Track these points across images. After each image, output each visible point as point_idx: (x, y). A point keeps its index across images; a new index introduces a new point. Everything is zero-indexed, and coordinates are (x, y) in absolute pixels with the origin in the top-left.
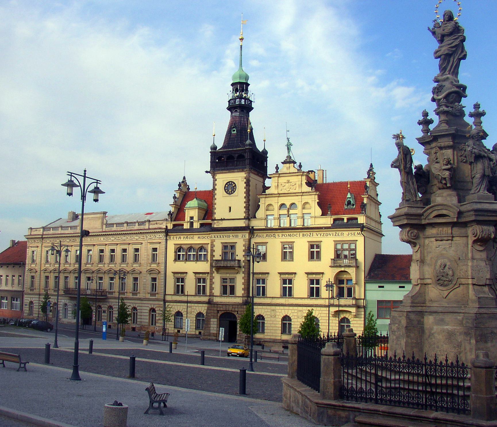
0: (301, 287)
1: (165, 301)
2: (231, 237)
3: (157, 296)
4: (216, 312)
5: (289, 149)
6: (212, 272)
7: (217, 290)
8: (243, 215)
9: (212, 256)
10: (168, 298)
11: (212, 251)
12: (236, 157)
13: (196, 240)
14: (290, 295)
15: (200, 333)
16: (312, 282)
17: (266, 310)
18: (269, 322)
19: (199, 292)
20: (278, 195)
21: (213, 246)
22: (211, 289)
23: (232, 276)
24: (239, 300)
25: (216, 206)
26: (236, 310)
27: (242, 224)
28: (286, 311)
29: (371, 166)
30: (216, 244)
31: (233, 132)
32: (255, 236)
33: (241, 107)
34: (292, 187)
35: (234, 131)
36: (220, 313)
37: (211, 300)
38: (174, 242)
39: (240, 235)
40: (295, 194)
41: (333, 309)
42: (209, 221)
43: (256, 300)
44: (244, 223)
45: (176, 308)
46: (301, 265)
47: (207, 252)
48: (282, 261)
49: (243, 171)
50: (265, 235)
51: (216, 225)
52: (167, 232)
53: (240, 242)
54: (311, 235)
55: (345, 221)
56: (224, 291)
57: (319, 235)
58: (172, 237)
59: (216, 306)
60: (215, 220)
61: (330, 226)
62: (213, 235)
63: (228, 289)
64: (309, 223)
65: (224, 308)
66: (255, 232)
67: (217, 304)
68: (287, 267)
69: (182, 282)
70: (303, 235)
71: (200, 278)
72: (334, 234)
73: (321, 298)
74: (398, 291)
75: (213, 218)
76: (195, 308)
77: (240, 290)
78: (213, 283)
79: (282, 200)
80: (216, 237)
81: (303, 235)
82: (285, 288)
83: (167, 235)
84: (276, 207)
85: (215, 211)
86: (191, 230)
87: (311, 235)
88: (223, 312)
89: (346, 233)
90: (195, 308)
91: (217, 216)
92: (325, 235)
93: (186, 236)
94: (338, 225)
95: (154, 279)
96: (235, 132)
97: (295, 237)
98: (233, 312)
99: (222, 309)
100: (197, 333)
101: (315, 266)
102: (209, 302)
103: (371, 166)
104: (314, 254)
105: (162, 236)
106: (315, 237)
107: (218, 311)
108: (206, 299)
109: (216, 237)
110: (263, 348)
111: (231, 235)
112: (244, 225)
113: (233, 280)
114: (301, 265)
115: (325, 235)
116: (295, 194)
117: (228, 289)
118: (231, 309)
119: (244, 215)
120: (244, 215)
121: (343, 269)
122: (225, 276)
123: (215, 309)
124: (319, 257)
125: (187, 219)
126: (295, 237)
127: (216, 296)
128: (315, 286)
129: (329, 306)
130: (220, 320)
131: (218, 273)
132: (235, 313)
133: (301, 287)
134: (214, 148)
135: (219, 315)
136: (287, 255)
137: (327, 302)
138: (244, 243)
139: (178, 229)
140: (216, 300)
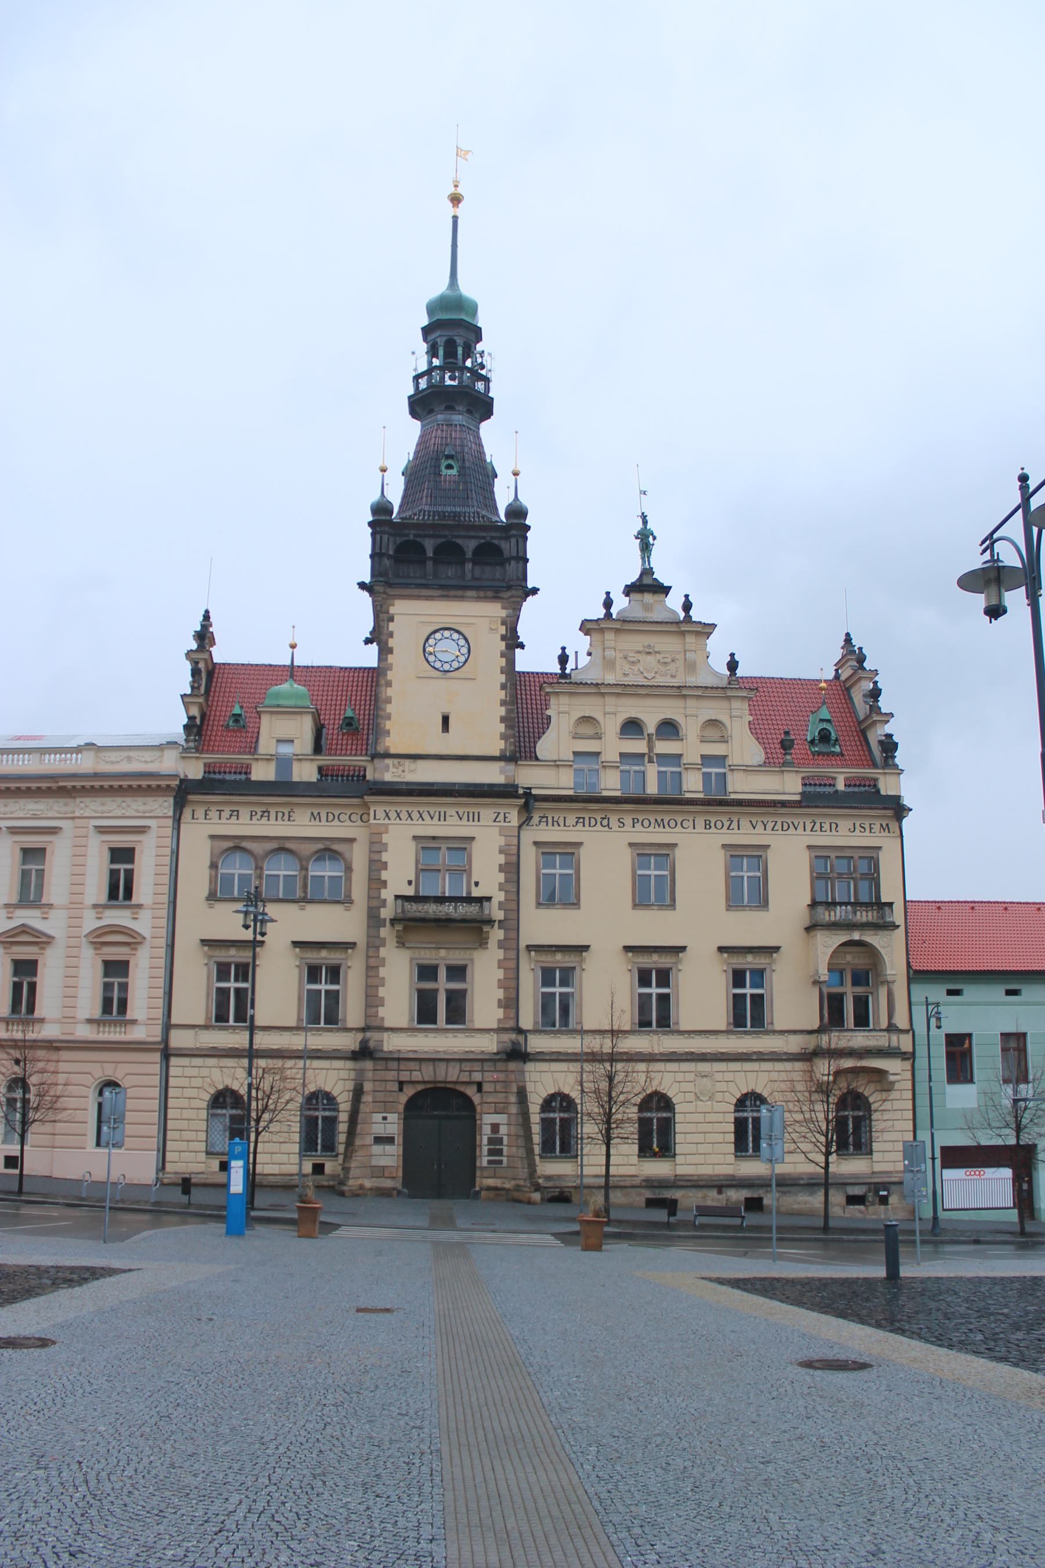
0: (702, 997)
1: (167, 1053)
2: (453, 820)
3: (138, 1034)
4: (395, 1087)
5: (646, 548)
6: (374, 944)
7: (398, 1003)
8: (496, 746)
9: (376, 883)
10: (179, 1039)
11: (376, 866)
12: (469, 554)
13: (303, 824)
14: (758, 1020)
15: (318, 1169)
16: (738, 978)
17: (680, 1077)
18: (690, 1117)
19: (221, 1017)
20: (684, 692)
21: (376, 847)
22: (372, 1000)
23: (456, 957)
24: (489, 1044)
25: (389, 708)
26: (477, 1077)
27: (493, 774)
28: (560, 1076)
29: (207, 616)
30: (398, 847)
31: (444, 472)
32: (536, 819)
33: (453, 389)
34: (663, 669)
35: (449, 467)
36: (410, 1091)
37: (372, 1044)
38: (202, 829)
39: (487, 814)
40: (680, 692)
41: (823, 1068)
42: (360, 760)
43: (537, 1043)
44: (501, 772)
45: (732, 1087)
46: (701, 922)
47: (349, 869)
48: (539, 905)
49: (496, 598)
50: (571, 819)
51: (391, 773)
52: (184, 793)
53: (487, 834)
54: (735, 825)
55: (841, 786)
56: (426, 1013)
57: (760, 828)
58: (200, 812)
59: (394, 1065)
60: (387, 755)
61: (798, 798)
62: (379, 809)
63: (439, 1003)
64: (740, 786)
65: (427, 1073)
66: (538, 804)
67: (399, 1059)
68: (654, 928)
69: (564, 983)
70: (707, 825)
71: (321, 965)
72: (809, 826)
73: (774, 1032)
74: (1003, 1004)
75: (381, 749)
76: (729, 1076)
77: (485, 1007)
78: (382, 982)
79: (631, 708)
80: (393, 815)
81: (707, 825)
82: (223, 993)
83: (180, 805)
84: (611, 727)
85: (388, 725)
86: (283, 789)
87: (735, 825)
88: (420, 1087)
89: (845, 825)
90: (729, 1076)
91: (394, 743)
92: (778, 826)
93: (259, 810)
94: (816, 799)
95: (116, 969)
96: (454, 472)
97: (679, 829)
98: (462, 1088)
99: (417, 1076)
100: (308, 1168)
101: (749, 929)
102: (364, 1053)
103: (207, 616)
104: (748, 890)
105: (165, 805)
106: (747, 832)
107: (401, 1084)
108: (347, 1042)
109: (393, 815)
110: (672, 1213)
111: (451, 811)
112: (500, 779)
113: (458, 972)
114: (701, 922)
115: (778, 826)
116: (680, 692)
117: (439, 1003)
118: (453, 1073)
119: (502, 744)
120: (502, 744)
121: (856, 936)
122: (428, 957)
123: (392, 1075)
124: (762, 902)
125: (267, 745)
126: (679, 829)
127: (392, 1030)
128: (232, 985)
129: (808, 1056)
130: (405, 1119)
131: (401, 944)
132: (471, 1091)
133: (702, 997)
134: (381, 509)
135: (403, 1098)
136: (654, 891)
137: (794, 1044)
138: (502, 841)
139: (223, 785)
140: (392, 1043)
